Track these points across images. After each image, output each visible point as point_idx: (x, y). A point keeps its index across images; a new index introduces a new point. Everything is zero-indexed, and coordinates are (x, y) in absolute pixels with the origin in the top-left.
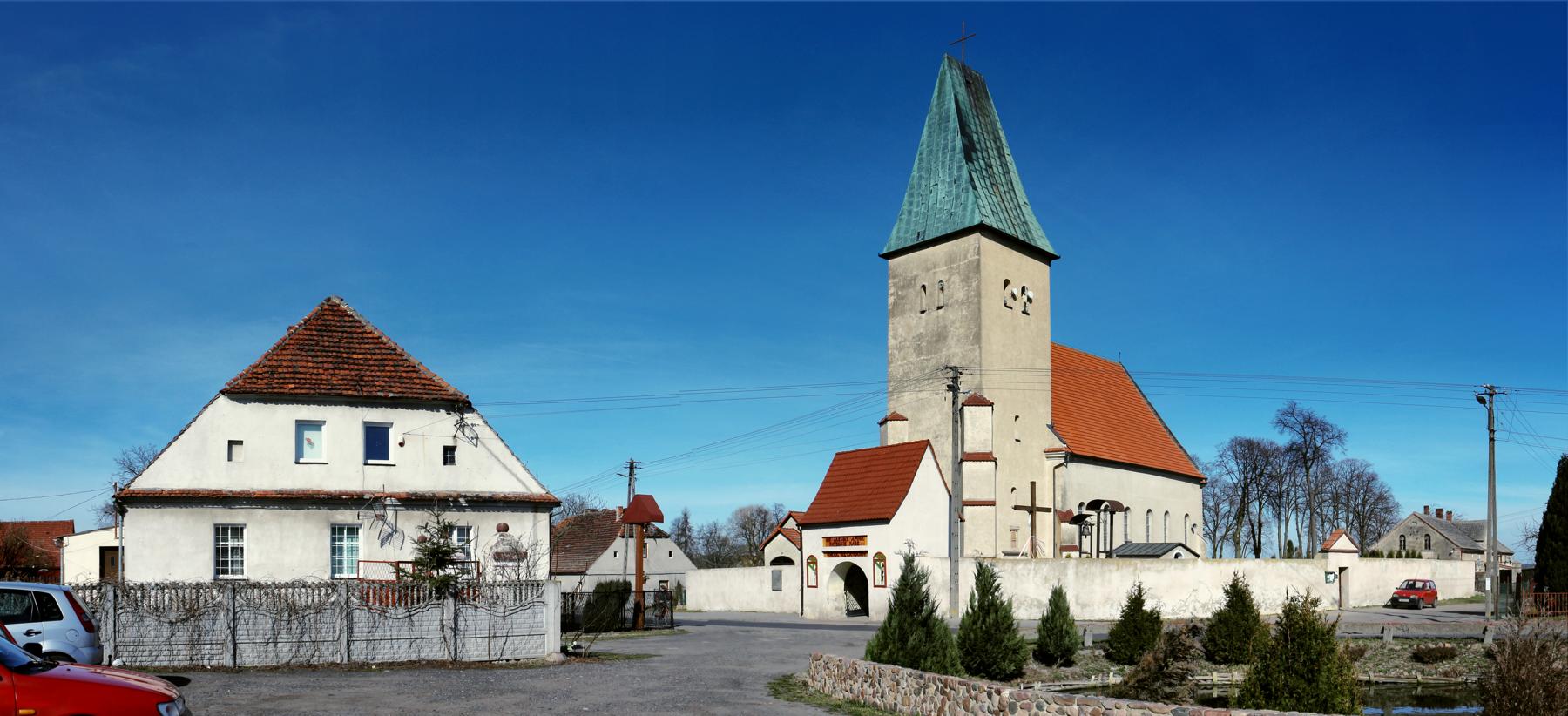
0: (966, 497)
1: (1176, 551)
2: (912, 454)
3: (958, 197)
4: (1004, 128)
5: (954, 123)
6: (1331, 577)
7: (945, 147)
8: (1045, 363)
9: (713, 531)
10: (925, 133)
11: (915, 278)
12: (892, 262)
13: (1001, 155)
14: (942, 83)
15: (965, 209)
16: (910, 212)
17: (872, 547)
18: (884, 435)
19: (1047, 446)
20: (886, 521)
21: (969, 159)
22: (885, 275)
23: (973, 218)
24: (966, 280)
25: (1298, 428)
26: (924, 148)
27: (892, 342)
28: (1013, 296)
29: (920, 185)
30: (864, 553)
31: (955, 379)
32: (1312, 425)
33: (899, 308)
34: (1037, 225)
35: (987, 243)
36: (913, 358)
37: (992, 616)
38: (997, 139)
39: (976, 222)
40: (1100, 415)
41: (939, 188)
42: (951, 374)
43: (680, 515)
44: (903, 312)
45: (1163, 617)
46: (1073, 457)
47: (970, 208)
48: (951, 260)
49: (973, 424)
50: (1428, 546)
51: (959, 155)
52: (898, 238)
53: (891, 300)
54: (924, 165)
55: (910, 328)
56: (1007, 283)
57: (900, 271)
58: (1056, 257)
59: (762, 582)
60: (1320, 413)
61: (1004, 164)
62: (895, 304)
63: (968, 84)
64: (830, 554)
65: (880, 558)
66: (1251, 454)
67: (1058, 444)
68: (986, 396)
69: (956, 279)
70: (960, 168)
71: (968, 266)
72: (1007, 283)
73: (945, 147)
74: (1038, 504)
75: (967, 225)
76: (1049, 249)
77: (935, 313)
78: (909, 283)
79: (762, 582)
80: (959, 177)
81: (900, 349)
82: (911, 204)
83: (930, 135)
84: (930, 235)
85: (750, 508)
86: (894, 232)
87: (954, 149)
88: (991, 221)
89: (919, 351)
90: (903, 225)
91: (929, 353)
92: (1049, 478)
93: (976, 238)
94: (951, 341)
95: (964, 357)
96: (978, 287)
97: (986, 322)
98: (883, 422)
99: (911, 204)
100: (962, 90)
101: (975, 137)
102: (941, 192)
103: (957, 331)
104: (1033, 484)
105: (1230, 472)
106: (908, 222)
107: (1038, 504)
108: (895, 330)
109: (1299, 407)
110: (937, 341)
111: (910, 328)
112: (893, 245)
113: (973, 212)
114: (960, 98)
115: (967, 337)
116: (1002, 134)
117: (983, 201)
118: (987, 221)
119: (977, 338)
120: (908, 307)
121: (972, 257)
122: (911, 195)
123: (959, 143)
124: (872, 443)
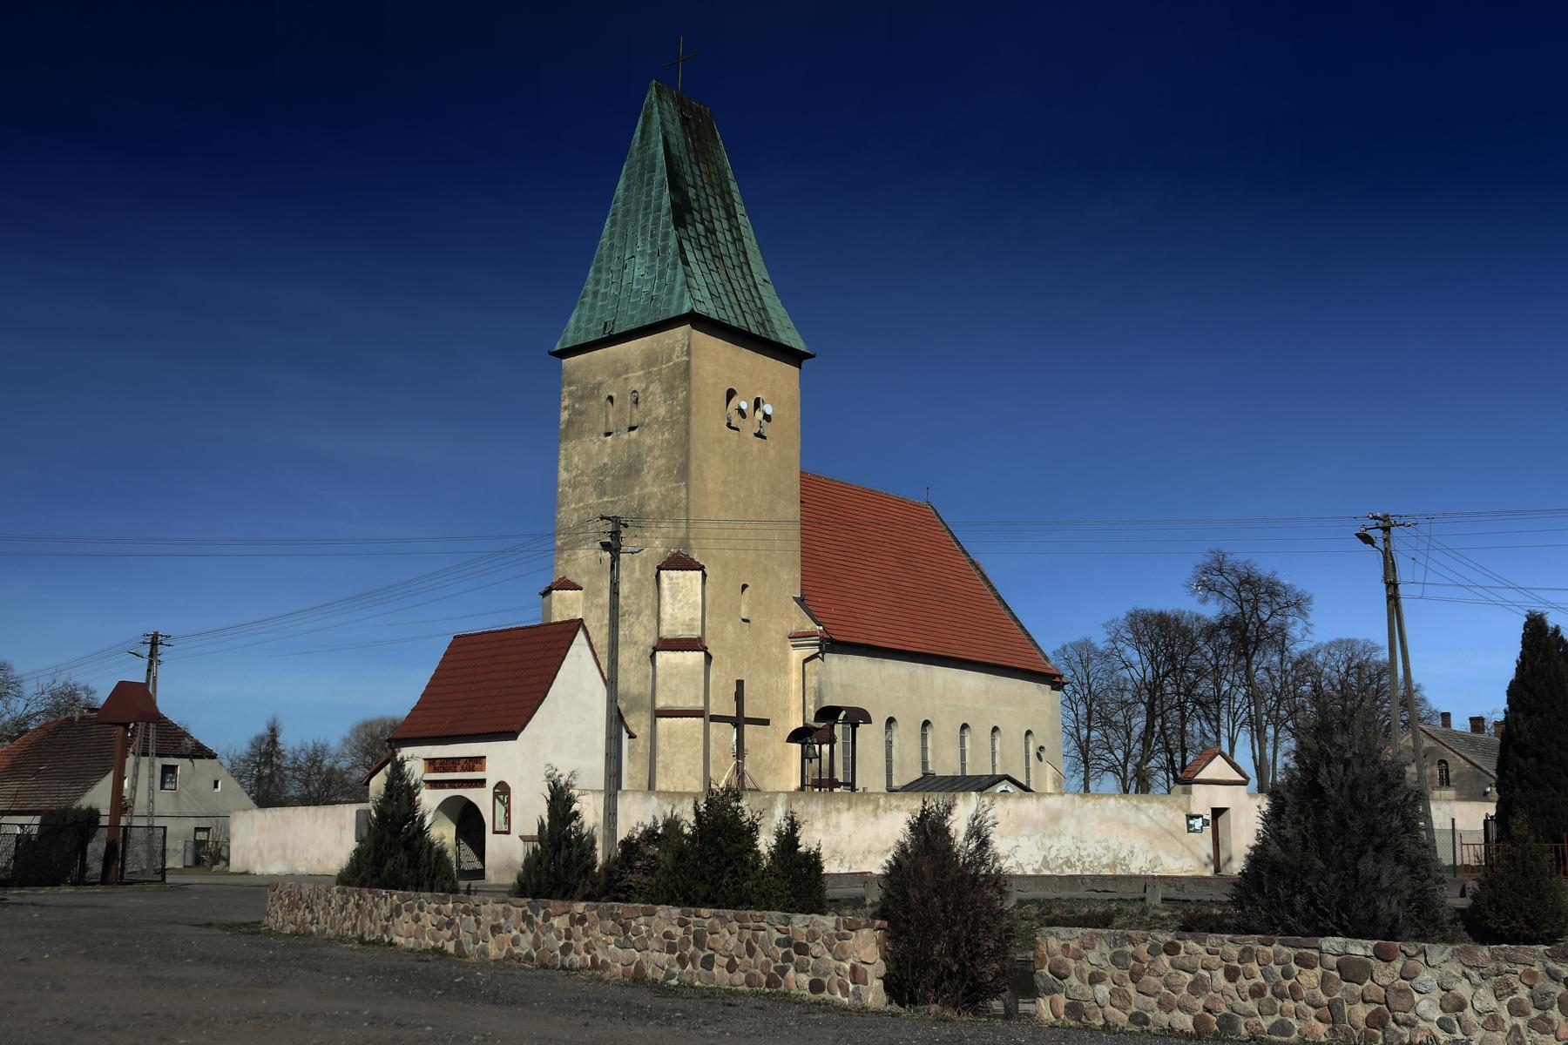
0: (661, 703)
1: (1000, 787)
2: (551, 643)
3: (662, 274)
4: (737, 179)
5: (661, 174)
6: (1198, 823)
7: (648, 206)
8: (791, 510)
9: (316, 756)
10: (621, 184)
11: (600, 384)
12: (568, 362)
13: (731, 216)
14: (647, 119)
15: (671, 291)
16: (595, 294)
17: (492, 774)
18: (548, 609)
19: (794, 628)
20: (512, 735)
21: (679, 221)
22: (558, 379)
23: (681, 305)
24: (669, 390)
25: (1230, 592)
26: (618, 205)
27: (563, 476)
28: (741, 412)
29: (610, 257)
30: (481, 783)
31: (615, 534)
32: (1254, 589)
33: (575, 428)
34: (782, 311)
35: (700, 337)
36: (593, 500)
37: (564, 853)
38: (725, 193)
39: (685, 310)
40: (882, 581)
41: (634, 259)
42: (610, 528)
43: (263, 730)
44: (580, 435)
45: (830, 867)
46: (832, 645)
47: (678, 289)
48: (650, 361)
49: (673, 596)
50: (1445, 782)
51: (666, 217)
52: (578, 329)
53: (565, 415)
54: (617, 229)
55: (589, 456)
56: (731, 394)
57: (579, 375)
58: (807, 356)
59: (342, 828)
60: (1266, 566)
61: (734, 227)
62: (570, 422)
63: (685, 121)
64: (435, 784)
65: (502, 790)
66: (1162, 634)
67: (810, 626)
68: (696, 557)
69: (656, 388)
70: (666, 235)
71: (672, 369)
72: (731, 394)
73: (648, 206)
74: (748, 714)
75: (673, 314)
76: (800, 345)
77: (625, 436)
78: (590, 393)
79: (342, 828)
80: (665, 248)
81: (574, 486)
82: (598, 282)
83: (627, 189)
84: (622, 327)
85: (382, 722)
86: (572, 320)
87: (659, 209)
88: (708, 308)
89: (601, 490)
90: (585, 312)
91: (616, 493)
92: (795, 677)
93: (681, 333)
94: (648, 477)
95: (664, 498)
96: (687, 400)
97: (697, 448)
98: (547, 592)
99: (598, 282)
100: (675, 129)
101: (692, 193)
102: (638, 269)
103: (655, 462)
104: (740, 684)
105: (1128, 666)
106: (593, 307)
107: (748, 714)
108: (569, 458)
109: (1230, 560)
110: (627, 476)
111: (589, 456)
112: (570, 337)
113: (682, 296)
114: (672, 140)
115: (670, 471)
116: (734, 186)
117: (699, 280)
118: (701, 309)
119: (684, 472)
120: (587, 426)
121: (678, 358)
122: (598, 270)
123: (666, 202)
124: (531, 618)
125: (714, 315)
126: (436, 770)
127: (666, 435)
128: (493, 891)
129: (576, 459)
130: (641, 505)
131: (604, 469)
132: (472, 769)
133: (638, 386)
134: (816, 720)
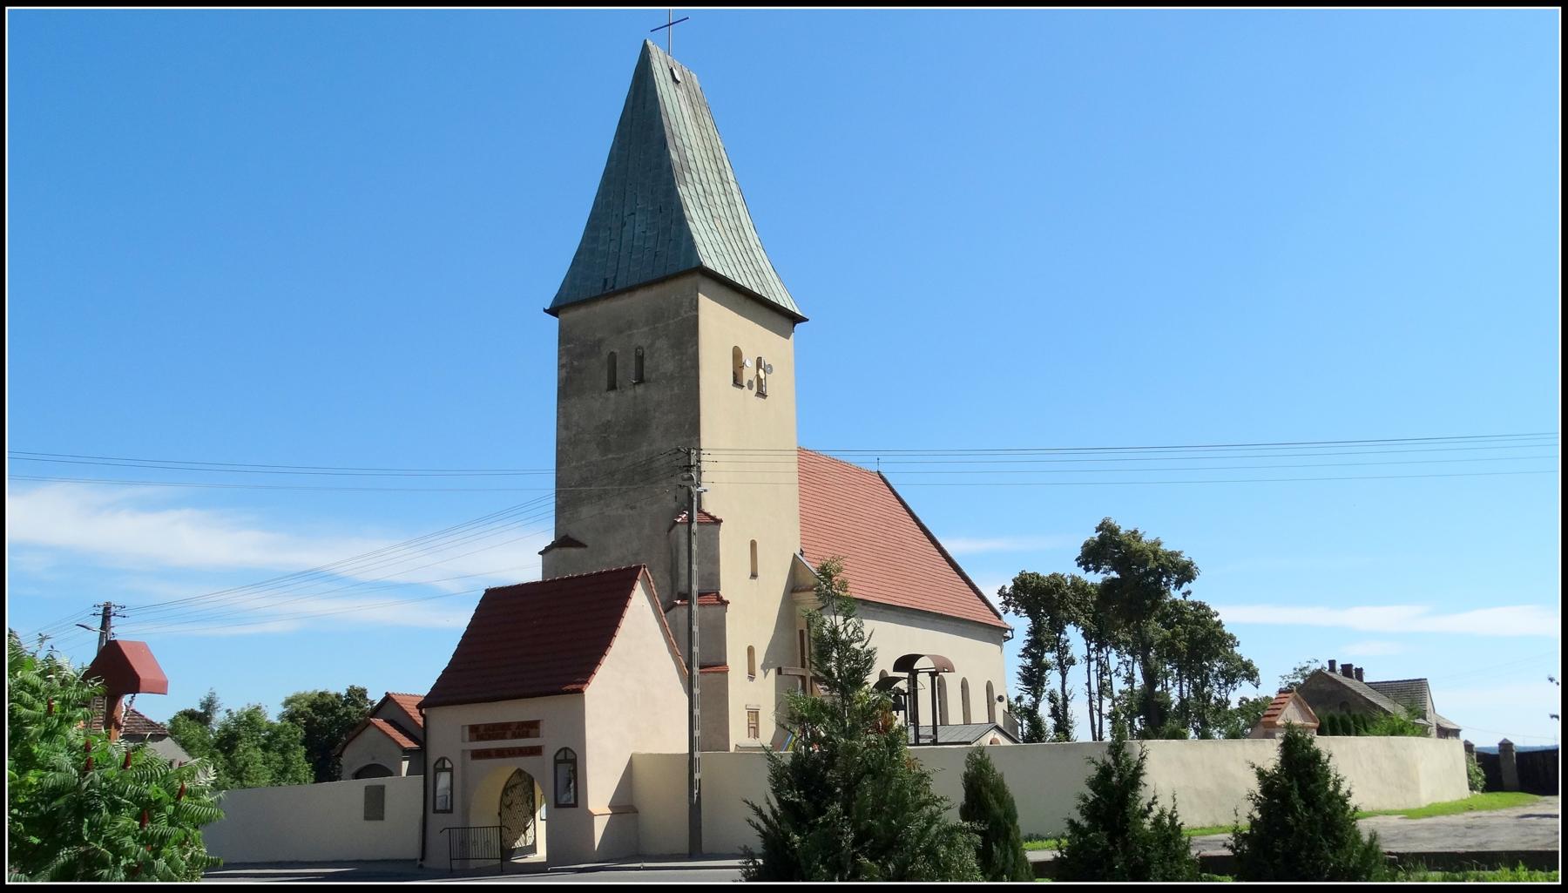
11: (601, 341)
30: (536, 751)
36: (596, 457)
69: (662, 343)
77: (630, 393)
89: (605, 446)
125: (720, 271)
126: (480, 738)
127: (676, 391)
128: (1197, 689)
129: (576, 418)
130: (651, 460)
131: (607, 426)
132: (527, 735)
133: (643, 342)
134: (895, 669)
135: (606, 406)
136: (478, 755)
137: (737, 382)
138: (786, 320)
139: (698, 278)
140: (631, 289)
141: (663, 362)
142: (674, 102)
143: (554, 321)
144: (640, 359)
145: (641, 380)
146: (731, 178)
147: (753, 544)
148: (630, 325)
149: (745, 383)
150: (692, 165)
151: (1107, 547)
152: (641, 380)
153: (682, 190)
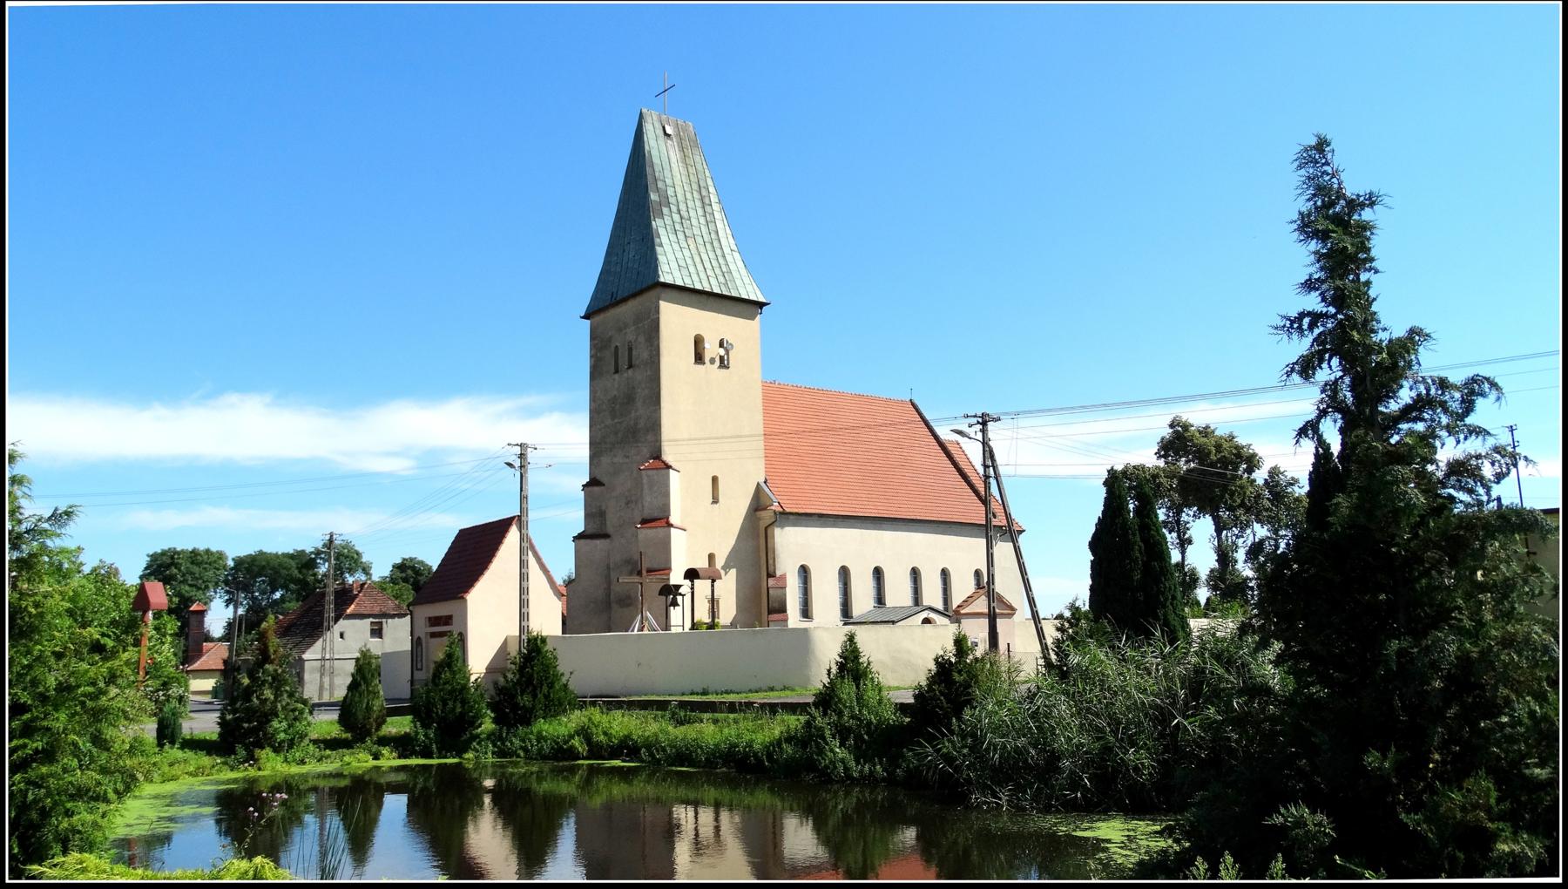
36: (609, 422)
69: (641, 339)
89: (613, 415)
131: (614, 400)
135: (615, 383)
136: (433, 635)
137: (699, 358)
138: (751, 308)
139: (658, 290)
140: (625, 300)
141: (642, 353)
142: (664, 155)
143: (588, 322)
144: (630, 350)
145: (630, 366)
146: (714, 199)
147: (715, 480)
148: (626, 326)
149: (707, 359)
150: (672, 200)
151: (1178, 442)
152: (630, 366)
153: (657, 224)
